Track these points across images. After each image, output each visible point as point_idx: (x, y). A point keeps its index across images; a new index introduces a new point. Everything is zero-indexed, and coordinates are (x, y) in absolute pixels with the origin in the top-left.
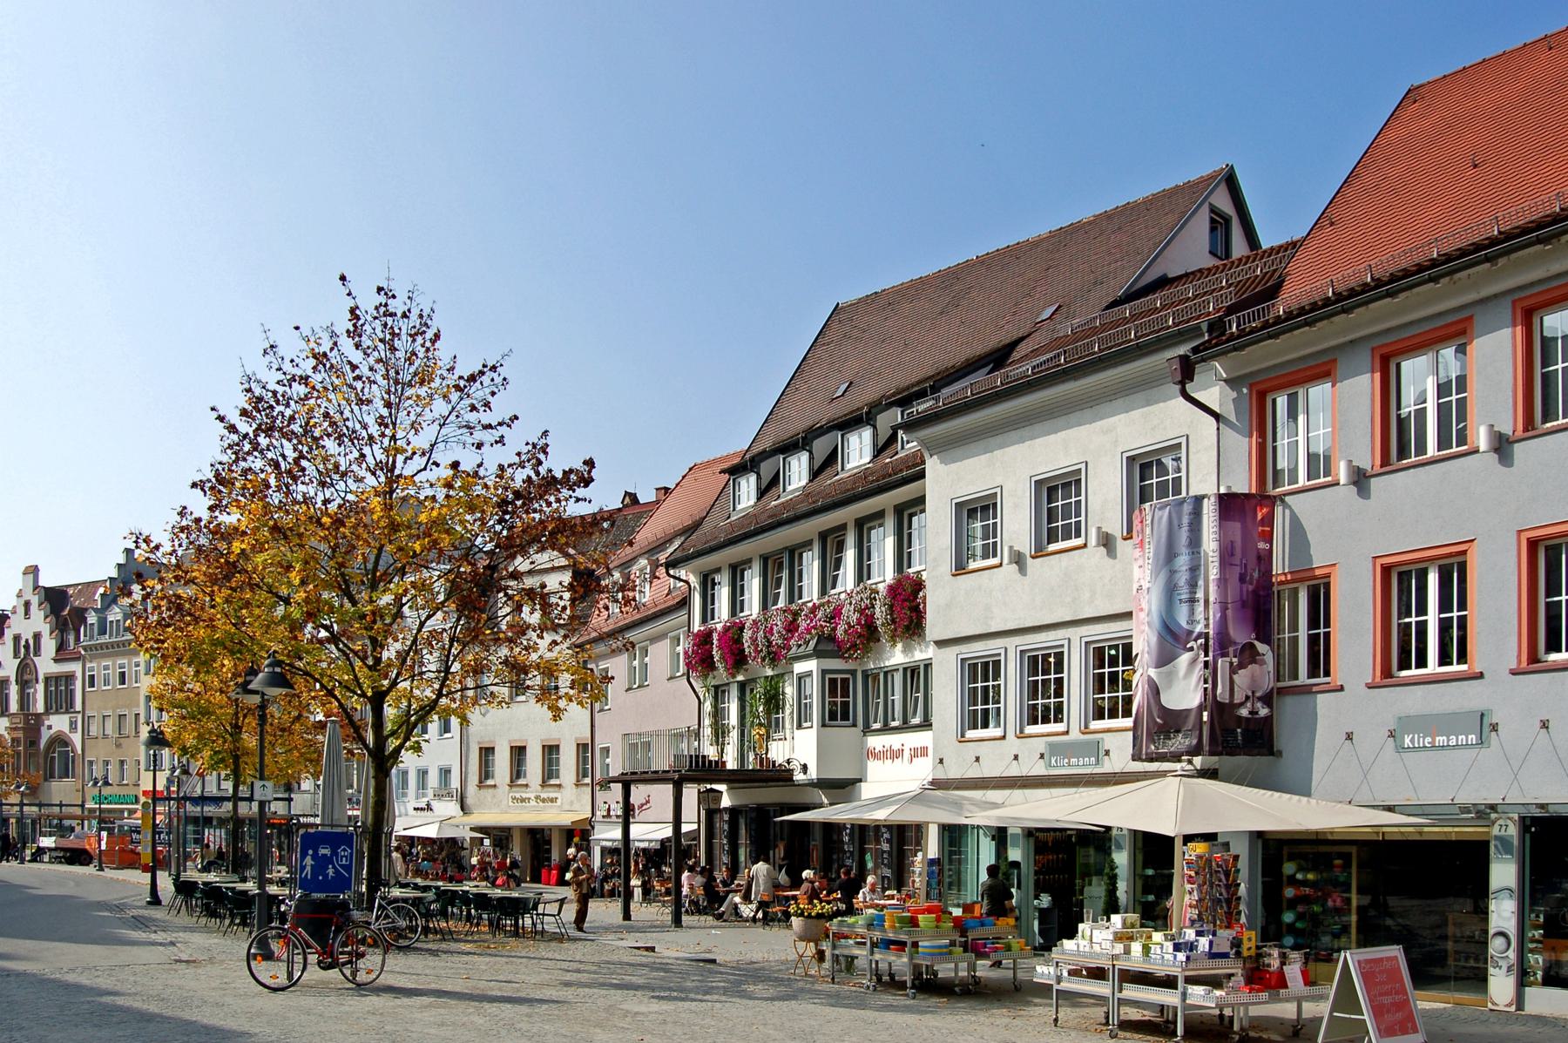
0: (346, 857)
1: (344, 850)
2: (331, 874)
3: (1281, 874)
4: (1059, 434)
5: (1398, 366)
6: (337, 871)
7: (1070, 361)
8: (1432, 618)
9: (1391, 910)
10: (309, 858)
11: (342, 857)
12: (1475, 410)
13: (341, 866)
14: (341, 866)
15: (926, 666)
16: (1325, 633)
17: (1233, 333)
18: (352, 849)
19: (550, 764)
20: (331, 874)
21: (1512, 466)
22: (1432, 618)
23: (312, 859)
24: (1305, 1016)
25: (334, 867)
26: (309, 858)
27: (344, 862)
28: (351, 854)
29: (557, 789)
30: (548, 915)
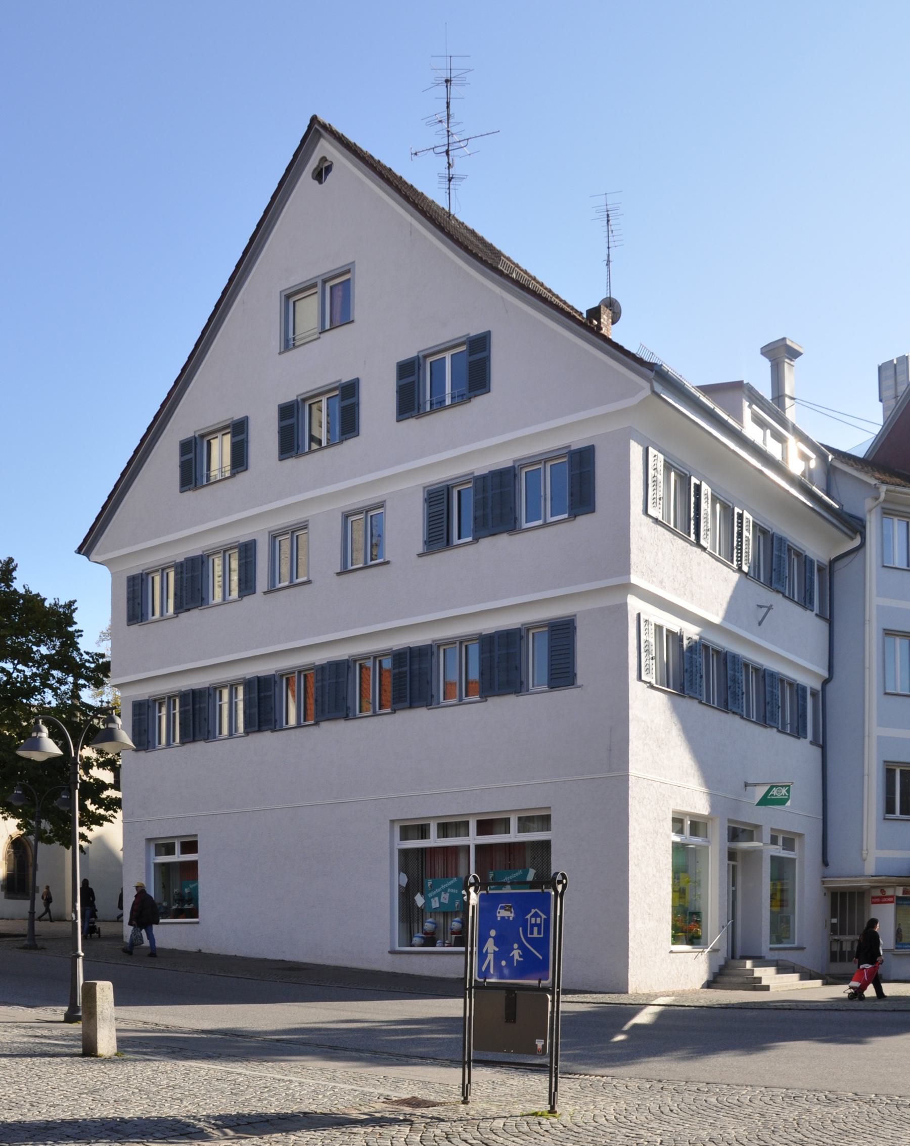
0: (539, 926)
1: (536, 915)
2: (517, 957)
3: (860, 986)
4: (630, 842)
6: (525, 952)
9: (870, 459)
10: (491, 942)
11: (532, 926)
12: (313, 1010)
13: (529, 940)
14: (531, 941)
17: (544, 919)
19: (507, 277)
20: (517, 957)
23: (496, 944)
25: (522, 947)
26: (491, 942)
27: (535, 935)
28: (547, 921)
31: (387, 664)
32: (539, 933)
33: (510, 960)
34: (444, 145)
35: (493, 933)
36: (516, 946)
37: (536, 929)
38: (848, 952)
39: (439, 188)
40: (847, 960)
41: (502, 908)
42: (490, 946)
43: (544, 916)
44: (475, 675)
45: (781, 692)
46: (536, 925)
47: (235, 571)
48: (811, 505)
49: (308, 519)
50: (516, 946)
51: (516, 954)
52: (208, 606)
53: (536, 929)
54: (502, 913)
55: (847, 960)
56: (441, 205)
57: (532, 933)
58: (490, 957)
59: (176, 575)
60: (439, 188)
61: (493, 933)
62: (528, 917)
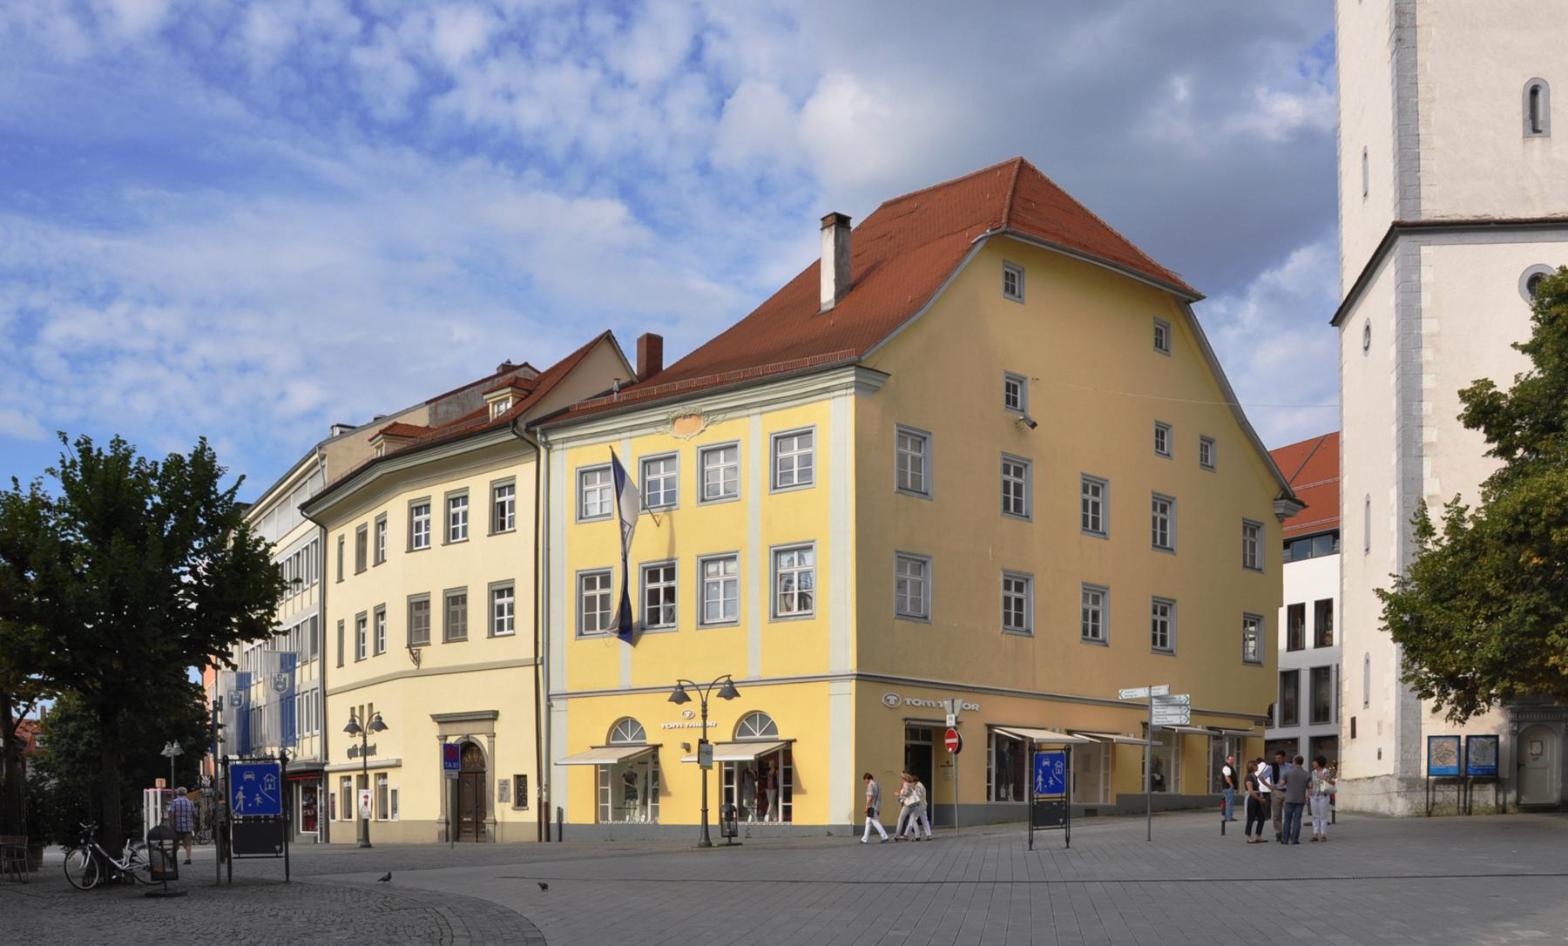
1: (270, 777)
10: (1040, 776)
11: (268, 784)
13: (267, 792)
23: (1043, 777)
25: (1053, 778)
31: (1309, 554)
32: (272, 786)
33: (1048, 784)
35: (241, 788)
37: (270, 785)
38: (176, 757)
40: (785, 804)
42: (240, 795)
47: (463, 406)
48: (1291, 832)
50: (257, 795)
51: (1051, 782)
52: (584, 588)
53: (270, 785)
54: (247, 777)
55: (785, 804)
57: (268, 787)
61: (241, 788)
62: (265, 778)
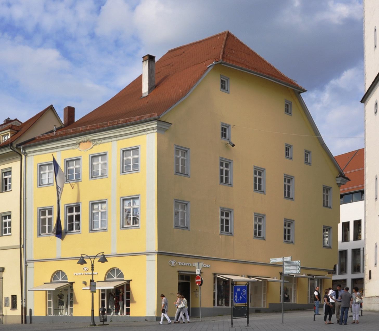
0: (245, 292)
1: (244, 290)
5: (69, 163)
6: (243, 298)
7: (128, 122)
8: (47, 225)
10: (236, 296)
13: (243, 295)
14: (243, 295)
15: (44, 231)
16: (49, 219)
18: (246, 290)
20: (241, 299)
21: (65, 109)
22: (47, 225)
23: (237, 296)
24: (96, 290)
25: (242, 297)
26: (236, 296)
27: (244, 294)
29: (186, 229)
30: (154, 260)
34: (343, 170)
36: (241, 296)
37: (244, 293)
39: (31, 323)
41: (238, 289)
43: (245, 290)
44: (236, 306)
45: (267, 286)
46: (244, 292)
49: (364, 273)
50: (241, 296)
51: (241, 298)
53: (244, 293)
55: (226, 225)
56: (155, 60)
57: (244, 293)
58: (236, 299)
59: (317, 282)
60: (31, 323)
62: (243, 291)
